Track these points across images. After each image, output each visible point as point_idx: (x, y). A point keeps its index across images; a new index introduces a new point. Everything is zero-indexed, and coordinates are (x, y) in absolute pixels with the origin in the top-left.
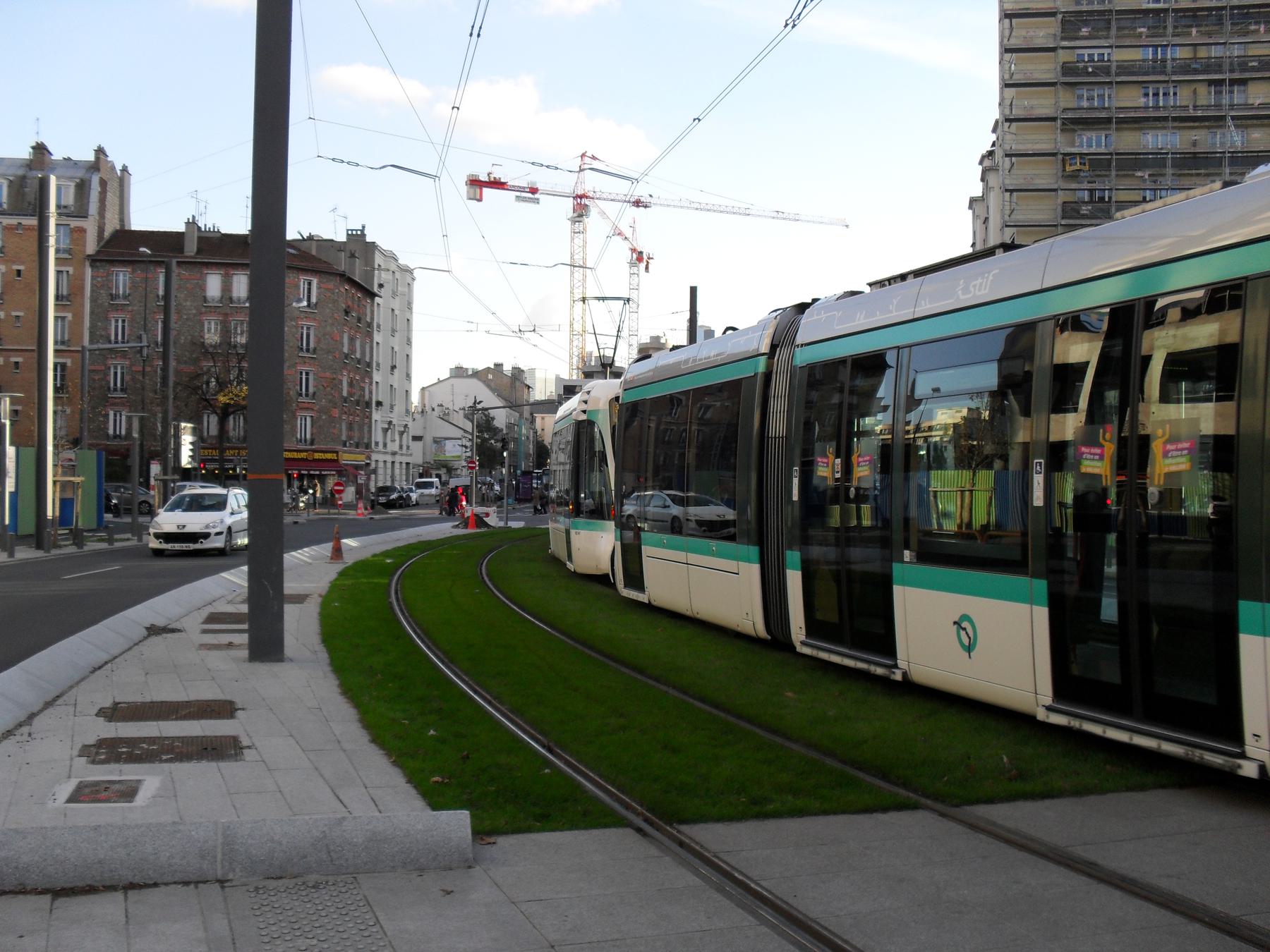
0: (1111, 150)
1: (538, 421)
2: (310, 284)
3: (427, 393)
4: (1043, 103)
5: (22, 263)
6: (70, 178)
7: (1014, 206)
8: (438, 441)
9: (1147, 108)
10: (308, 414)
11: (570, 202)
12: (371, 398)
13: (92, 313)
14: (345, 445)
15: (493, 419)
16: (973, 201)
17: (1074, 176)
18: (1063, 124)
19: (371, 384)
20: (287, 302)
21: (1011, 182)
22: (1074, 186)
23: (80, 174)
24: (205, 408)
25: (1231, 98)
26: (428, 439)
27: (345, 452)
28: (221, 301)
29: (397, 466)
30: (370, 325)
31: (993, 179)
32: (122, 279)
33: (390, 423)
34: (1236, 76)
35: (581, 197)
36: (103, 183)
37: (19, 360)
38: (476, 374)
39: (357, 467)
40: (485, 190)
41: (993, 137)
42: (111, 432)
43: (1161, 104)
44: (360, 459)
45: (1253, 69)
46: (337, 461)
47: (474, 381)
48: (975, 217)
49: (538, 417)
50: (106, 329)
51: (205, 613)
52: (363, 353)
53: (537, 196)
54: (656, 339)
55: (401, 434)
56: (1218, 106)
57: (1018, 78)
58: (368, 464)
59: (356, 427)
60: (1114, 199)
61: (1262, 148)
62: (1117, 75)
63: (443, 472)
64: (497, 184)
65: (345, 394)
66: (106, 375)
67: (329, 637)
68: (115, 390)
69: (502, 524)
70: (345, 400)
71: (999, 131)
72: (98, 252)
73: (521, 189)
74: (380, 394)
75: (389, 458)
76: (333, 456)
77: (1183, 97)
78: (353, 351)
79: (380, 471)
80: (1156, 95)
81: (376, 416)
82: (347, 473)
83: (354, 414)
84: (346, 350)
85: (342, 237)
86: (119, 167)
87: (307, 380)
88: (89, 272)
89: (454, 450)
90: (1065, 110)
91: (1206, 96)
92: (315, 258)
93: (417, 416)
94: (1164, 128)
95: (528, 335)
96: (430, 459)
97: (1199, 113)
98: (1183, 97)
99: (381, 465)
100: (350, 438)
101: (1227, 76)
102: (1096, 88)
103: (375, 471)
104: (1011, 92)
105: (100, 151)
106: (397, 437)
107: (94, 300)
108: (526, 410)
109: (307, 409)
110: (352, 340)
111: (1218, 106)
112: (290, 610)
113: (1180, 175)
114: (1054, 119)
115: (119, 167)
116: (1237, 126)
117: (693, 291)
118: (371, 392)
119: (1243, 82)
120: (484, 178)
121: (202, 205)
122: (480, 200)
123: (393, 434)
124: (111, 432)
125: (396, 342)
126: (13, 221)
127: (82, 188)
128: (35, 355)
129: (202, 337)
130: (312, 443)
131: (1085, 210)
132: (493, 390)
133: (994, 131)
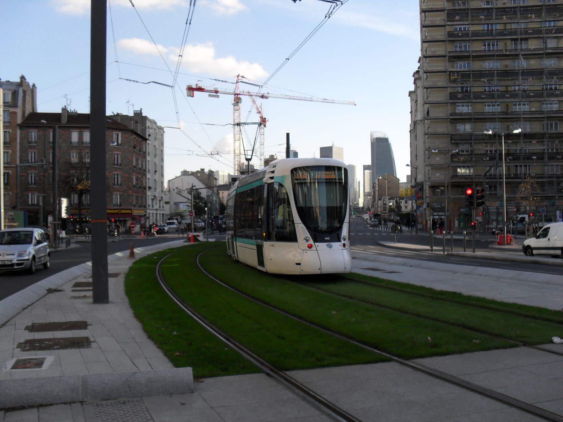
0: (470, 69)
2: (118, 135)
3: (171, 183)
4: (440, 50)
6: (9, 90)
8: (177, 204)
9: (485, 51)
10: (118, 193)
11: (232, 97)
13: (20, 150)
14: (135, 206)
15: (201, 193)
16: (410, 93)
17: (454, 81)
18: (449, 58)
19: (146, 179)
21: (427, 84)
22: (454, 85)
23: (14, 88)
25: (522, 46)
26: (172, 203)
27: (135, 210)
29: (158, 215)
30: (145, 153)
31: (419, 83)
32: (34, 134)
33: (155, 196)
34: (523, 36)
35: (237, 94)
36: (24, 92)
40: (195, 92)
41: (419, 65)
42: (30, 203)
43: (491, 49)
44: (142, 212)
45: (530, 34)
46: (131, 214)
49: (221, 192)
50: (27, 157)
52: (142, 165)
53: (218, 94)
55: (160, 201)
56: (516, 50)
57: (429, 38)
58: (145, 215)
59: (140, 198)
60: (472, 91)
62: (472, 37)
63: (179, 217)
64: (200, 89)
65: (134, 183)
66: (27, 177)
69: (205, 240)
70: (135, 186)
72: (23, 123)
73: (211, 91)
74: (150, 183)
75: (155, 212)
78: (137, 164)
80: (489, 45)
81: (149, 193)
82: (136, 219)
84: (134, 164)
85: (132, 114)
86: (31, 85)
87: (117, 178)
88: (18, 131)
90: (450, 52)
91: (510, 46)
92: (120, 123)
93: (167, 193)
94: (492, 60)
96: (173, 212)
97: (508, 53)
99: (151, 215)
100: (137, 203)
101: (519, 37)
102: (463, 42)
103: (148, 218)
104: (426, 45)
105: (23, 78)
106: (158, 203)
107: (21, 144)
108: (215, 189)
109: (118, 191)
110: (137, 159)
111: (516, 50)
112: (111, 281)
113: (500, 80)
114: (445, 56)
115: (31, 85)
116: (524, 59)
117: (288, 135)
118: (146, 183)
119: (526, 39)
120: (194, 87)
121: (69, 101)
122: (193, 96)
123: (156, 201)
124: (30, 203)
125: (157, 160)
131: (459, 96)
132: (200, 181)
133: (419, 62)
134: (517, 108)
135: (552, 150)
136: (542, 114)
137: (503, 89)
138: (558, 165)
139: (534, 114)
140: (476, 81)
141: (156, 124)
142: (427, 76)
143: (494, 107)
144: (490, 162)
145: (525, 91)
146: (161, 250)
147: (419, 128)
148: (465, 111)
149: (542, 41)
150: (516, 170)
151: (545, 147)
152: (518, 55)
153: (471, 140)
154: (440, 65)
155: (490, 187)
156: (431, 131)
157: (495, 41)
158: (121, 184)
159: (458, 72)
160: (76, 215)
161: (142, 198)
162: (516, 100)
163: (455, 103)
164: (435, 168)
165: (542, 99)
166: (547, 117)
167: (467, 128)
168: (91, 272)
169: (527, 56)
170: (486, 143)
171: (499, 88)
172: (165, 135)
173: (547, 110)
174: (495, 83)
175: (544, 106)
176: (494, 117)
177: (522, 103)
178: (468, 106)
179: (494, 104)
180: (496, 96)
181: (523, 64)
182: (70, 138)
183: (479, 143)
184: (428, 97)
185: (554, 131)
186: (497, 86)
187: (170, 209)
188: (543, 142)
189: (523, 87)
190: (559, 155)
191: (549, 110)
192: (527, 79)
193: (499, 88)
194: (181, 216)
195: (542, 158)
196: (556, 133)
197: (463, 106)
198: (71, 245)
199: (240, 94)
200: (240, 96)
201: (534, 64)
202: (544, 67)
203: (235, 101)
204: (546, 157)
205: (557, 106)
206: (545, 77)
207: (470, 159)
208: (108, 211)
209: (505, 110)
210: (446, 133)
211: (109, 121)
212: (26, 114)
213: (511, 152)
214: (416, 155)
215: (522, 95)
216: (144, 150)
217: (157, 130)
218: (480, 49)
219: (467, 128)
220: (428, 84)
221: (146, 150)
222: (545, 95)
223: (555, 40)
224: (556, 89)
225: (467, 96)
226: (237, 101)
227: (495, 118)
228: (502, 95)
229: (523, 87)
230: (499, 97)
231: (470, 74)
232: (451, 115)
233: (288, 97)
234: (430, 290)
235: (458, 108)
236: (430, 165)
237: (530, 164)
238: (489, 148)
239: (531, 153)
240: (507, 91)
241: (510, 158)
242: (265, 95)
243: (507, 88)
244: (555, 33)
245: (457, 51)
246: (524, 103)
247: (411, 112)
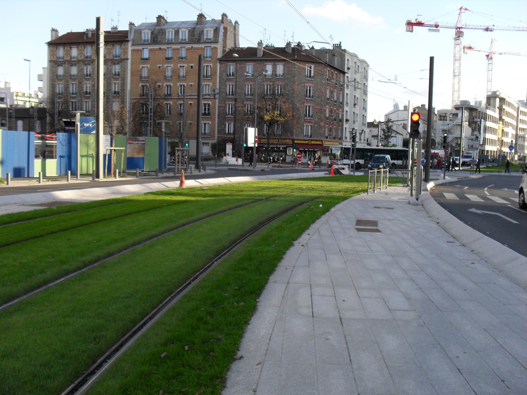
2: (310, 68)
5: (193, 63)
6: (212, 27)
10: (309, 124)
11: (454, 31)
12: (343, 118)
13: (220, 82)
14: (327, 138)
19: (343, 111)
23: (216, 25)
27: (327, 141)
28: (272, 76)
32: (232, 68)
35: (459, 28)
36: (225, 29)
37: (192, 102)
40: (414, 27)
42: (227, 132)
50: (225, 89)
52: (338, 98)
53: (438, 29)
54: (495, 93)
59: (334, 131)
64: (420, 24)
65: (327, 115)
66: (225, 108)
68: (229, 114)
70: (328, 119)
72: (222, 57)
73: (431, 26)
76: (321, 143)
81: (345, 125)
83: (333, 125)
84: (328, 96)
86: (233, 22)
87: (309, 110)
88: (218, 65)
105: (224, 15)
107: (220, 77)
109: (309, 122)
110: (332, 92)
115: (233, 22)
117: (432, 59)
118: (343, 115)
120: (413, 21)
122: (412, 31)
124: (227, 132)
126: (189, 46)
127: (216, 31)
128: (197, 100)
130: (311, 137)
146: (346, 183)
161: (337, 131)
199: (462, 28)
200: (462, 30)
212: (227, 50)
216: (341, 83)
217: (358, 64)
226: (459, 34)
233: (517, 29)
242: (489, 28)
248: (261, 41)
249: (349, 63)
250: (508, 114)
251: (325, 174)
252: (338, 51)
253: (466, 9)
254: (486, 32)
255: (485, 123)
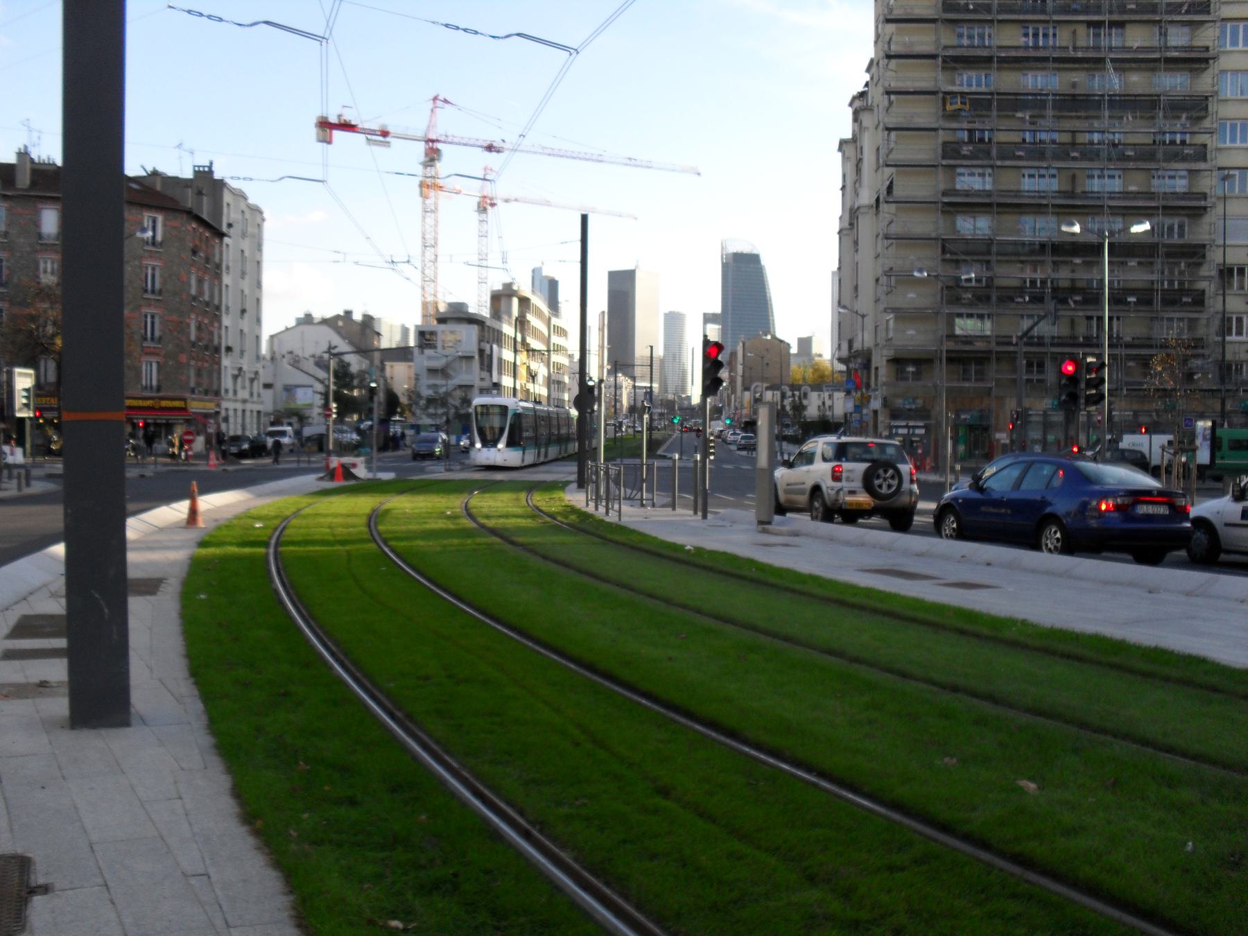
0: (992, 88)
1: (388, 369)
2: (154, 221)
3: (276, 340)
4: (923, 40)
7: (892, 145)
8: (289, 389)
9: (1026, 47)
10: (154, 360)
11: (421, 147)
12: (220, 344)
15: (349, 364)
16: (843, 143)
17: (954, 116)
18: (944, 61)
19: (220, 328)
20: (127, 231)
21: (892, 121)
22: (955, 125)
24: (42, 352)
25: (1110, 41)
26: (279, 386)
27: (194, 399)
29: (248, 414)
30: (218, 266)
31: (867, 119)
33: (240, 369)
34: (1116, 17)
35: (433, 141)
38: (325, 322)
39: (207, 416)
41: (867, 77)
43: (1041, 43)
44: (210, 407)
45: (1132, 11)
46: (184, 410)
47: (325, 328)
48: (845, 159)
49: (388, 364)
51: (13, 618)
52: (212, 296)
53: (388, 139)
55: (252, 380)
56: (1097, 48)
57: (898, 13)
58: (218, 413)
59: (204, 373)
60: (995, 140)
61: (1140, 92)
62: (999, 12)
63: (294, 420)
64: (347, 127)
65: (193, 337)
67: (201, 667)
69: (370, 476)
70: (194, 344)
71: (874, 69)
73: (372, 132)
74: (229, 339)
75: (239, 406)
77: (1063, 38)
78: (201, 292)
79: (231, 420)
80: (1036, 35)
81: (226, 362)
82: (197, 423)
84: (193, 291)
85: (188, 174)
89: (308, 398)
90: (945, 47)
91: (1085, 38)
92: (158, 193)
93: (269, 364)
94: (1044, 69)
95: (401, 266)
96: (281, 407)
97: (1080, 55)
98: (1063, 38)
99: (231, 413)
100: (199, 384)
101: (1106, 18)
102: (976, 26)
103: (226, 419)
104: (891, 28)
106: (247, 383)
108: (377, 355)
110: (200, 281)
111: (1097, 48)
112: (137, 606)
113: (1059, 117)
114: (933, 57)
116: (1115, 69)
117: (584, 219)
118: (220, 337)
119: (1121, 25)
120: (333, 119)
121: (35, 135)
122: (330, 142)
123: (244, 381)
125: (246, 285)
129: (38, 277)
130: (159, 389)
131: (966, 150)
132: (344, 338)
133: (868, 70)
134: (1096, 185)
135: (1171, 282)
136: (1152, 199)
137: (1066, 138)
138: (1180, 319)
139: (1135, 198)
140: (1007, 116)
141: (246, 199)
142: (891, 103)
143: (1041, 180)
144: (1031, 306)
145: (1115, 145)
147: (867, 225)
148: (977, 187)
149: (1156, 30)
150: (1089, 327)
151: (1154, 277)
152: (1100, 61)
153: (989, 253)
154: (923, 77)
155: (1030, 365)
156: (895, 229)
157: (1051, 25)
158: (160, 338)
159: (962, 94)
160: (51, 409)
161: (210, 373)
162: (1096, 164)
163: (955, 166)
164: (903, 315)
165: (1153, 165)
166: (1165, 208)
167: (975, 226)
168: (63, 580)
169: (1124, 64)
170: (1022, 262)
171: (1056, 136)
172: (267, 226)
173: (1162, 190)
174: (1047, 123)
175: (1155, 182)
176: (1044, 202)
177: (1106, 172)
178: (982, 175)
179: (1043, 172)
180: (1048, 154)
181: (1112, 82)
182: (37, 224)
183: (1007, 261)
184: (891, 151)
185: (1176, 239)
186: (1050, 133)
187: (275, 402)
188: (1151, 263)
189: (1111, 137)
190: (1188, 295)
191: (1168, 190)
192: (1121, 118)
193: (1056, 136)
194: (300, 417)
195: (1149, 302)
196: (1182, 246)
197: (972, 174)
198: (33, 483)
199: (437, 141)
200: (439, 146)
201: (1137, 82)
202: (1157, 90)
203: (426, 155)
204: (1158, 298)
205: (1184, 182)
206: (1161, 114)
207: (985, 297)
208: (129, 402)
209: (1069, 188)
210: (933, 235)
211: (134, 186)
213: (1079, 284)
214: (856, 288)
215: (1109, 154)
217: (247, 215)
218: (1015, 43)
219: (975, 226)
220: (894, 120)
221: (221, 260)
222: (1160, 155)
223: (1186, 30)
224: (1183, 142)
225: (981, 151)
226: (432, 156)
227: (1047, 206)
228: (1063, 152)
229: (1111, 137)
230: (1057, 157)
231: (990, 101)
232: (944, 194)
234: (1120, 647)
235: (962, 178)
236: (895, 310)
237: (1121, 314)
238: (1028, 274)
239: (1123, 289)
240: (1073, 144)
241: (1078, 298)
243: (1074, 138)
244: (1188, 12)
245: (961, 46)
246: (1111, 173)
247: (843, 188)
248: (26, 147)
249: (230, 214)
250: (537, 334)
251: (422, 471)
252: (207, 183)
253: (446, 101)
254: (487, 154)
255: (500, 352)
